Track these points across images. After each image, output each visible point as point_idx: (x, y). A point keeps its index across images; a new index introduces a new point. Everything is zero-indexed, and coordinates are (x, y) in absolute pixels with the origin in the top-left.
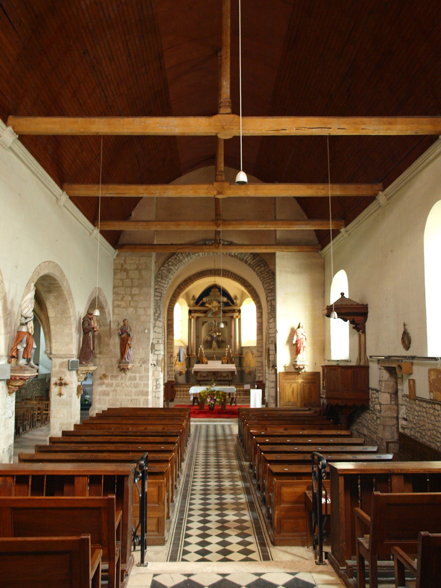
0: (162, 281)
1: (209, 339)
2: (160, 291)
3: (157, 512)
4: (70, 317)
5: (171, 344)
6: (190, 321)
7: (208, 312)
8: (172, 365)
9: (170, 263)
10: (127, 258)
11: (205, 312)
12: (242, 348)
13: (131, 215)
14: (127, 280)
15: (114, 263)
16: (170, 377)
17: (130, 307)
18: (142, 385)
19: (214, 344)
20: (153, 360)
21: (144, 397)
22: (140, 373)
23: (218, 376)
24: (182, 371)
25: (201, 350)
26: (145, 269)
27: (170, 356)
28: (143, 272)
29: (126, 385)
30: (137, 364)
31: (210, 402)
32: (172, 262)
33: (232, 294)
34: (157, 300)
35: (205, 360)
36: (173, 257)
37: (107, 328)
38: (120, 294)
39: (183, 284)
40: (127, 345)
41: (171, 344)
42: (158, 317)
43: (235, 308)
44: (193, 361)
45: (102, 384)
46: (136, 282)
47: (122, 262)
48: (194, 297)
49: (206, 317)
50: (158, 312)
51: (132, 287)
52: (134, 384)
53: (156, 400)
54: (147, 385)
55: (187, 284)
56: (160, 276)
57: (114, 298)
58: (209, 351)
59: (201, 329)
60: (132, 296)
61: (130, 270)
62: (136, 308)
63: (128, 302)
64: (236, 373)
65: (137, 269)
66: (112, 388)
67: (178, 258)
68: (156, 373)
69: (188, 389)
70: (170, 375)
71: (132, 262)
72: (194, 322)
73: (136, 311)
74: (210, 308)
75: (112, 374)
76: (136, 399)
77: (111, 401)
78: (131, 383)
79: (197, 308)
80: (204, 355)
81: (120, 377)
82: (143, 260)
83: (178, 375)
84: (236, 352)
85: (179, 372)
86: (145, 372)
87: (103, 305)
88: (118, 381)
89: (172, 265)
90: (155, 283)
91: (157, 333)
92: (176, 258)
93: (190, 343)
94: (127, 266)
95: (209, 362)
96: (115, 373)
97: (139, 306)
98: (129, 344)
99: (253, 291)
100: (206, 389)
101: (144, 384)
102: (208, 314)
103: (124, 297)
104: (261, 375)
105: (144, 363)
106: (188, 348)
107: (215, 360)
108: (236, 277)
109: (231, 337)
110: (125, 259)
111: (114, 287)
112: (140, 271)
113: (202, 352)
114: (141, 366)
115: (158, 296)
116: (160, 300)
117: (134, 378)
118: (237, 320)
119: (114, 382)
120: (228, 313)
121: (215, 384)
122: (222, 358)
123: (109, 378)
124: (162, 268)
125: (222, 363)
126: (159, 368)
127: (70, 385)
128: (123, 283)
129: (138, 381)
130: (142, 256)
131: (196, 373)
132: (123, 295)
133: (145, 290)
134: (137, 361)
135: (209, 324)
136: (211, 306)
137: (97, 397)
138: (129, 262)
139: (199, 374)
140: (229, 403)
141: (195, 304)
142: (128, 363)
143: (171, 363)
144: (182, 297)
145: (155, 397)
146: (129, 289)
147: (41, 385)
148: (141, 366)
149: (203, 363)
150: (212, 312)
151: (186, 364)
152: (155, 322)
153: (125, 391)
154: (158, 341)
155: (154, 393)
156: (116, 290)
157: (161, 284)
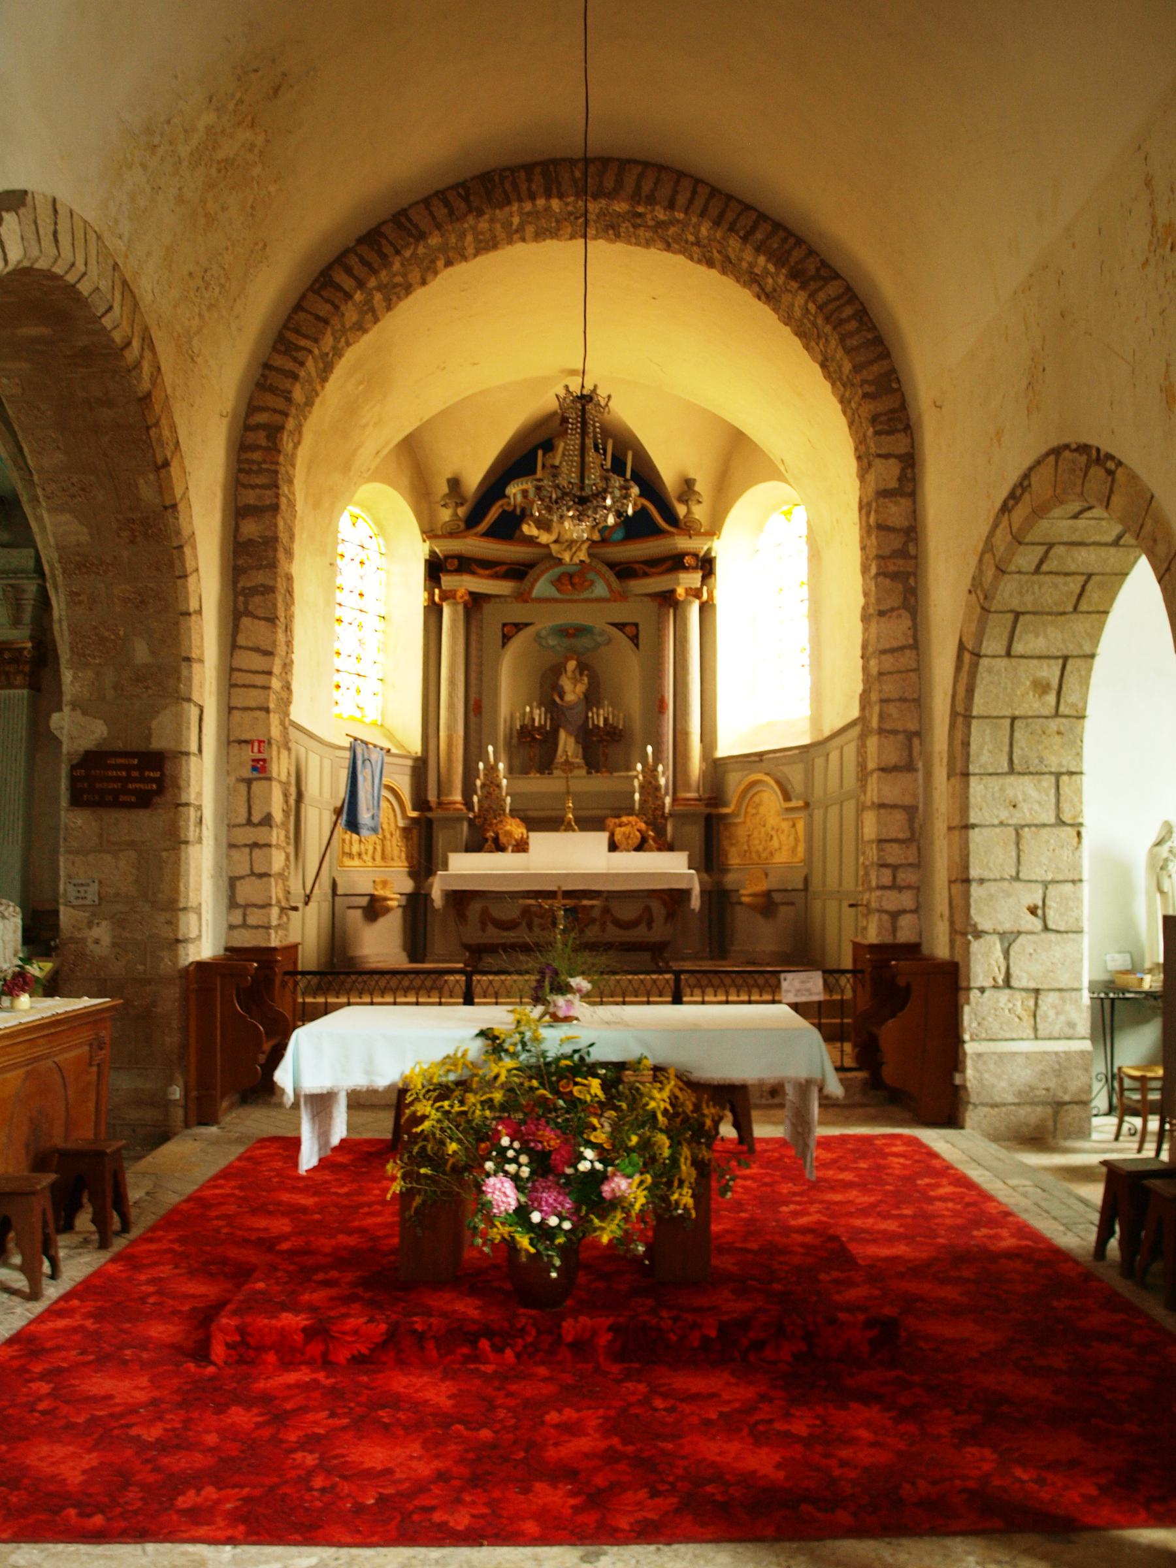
1: (539, 716)
5: (259, 680)
6: (433, 619)
7: (532, 574)
8: (259, 835)
11: (518, 572)
12: (717, 768)
16: (244, 925)
19: (567, 744)
24: (380, 892)
25: (492, 769)
27: (247, 773)
31: (522, 1212)
33: (668, 475)
35: (516, 829)
39: (353, 260)
41: (259, 680)
43: (683, 543)
44: (441, 838)
48: (455, 484)
49: (522, 597)
55: (386, 262)
58: (536, 784)
64: (695, 903)
72: (454, 621)
74: (547, 546)
79: (473, 545)
80: (508, 799)
84: (687, 787)
85: (364, 901)
93: (432, 746)
95: (537, 840)
99: (848, 311)
100: (475, 1048)
102: (536, 580)
104: (906, 900)
106: (420, 769)
107: (569, 828)
108: (730, 216)
109: (661, 706)
113: (499, 786)
118: (694, 612)
120: (646, 575)
121: (580, 982)
122: (611, 822)
125: (613, 847)
131: (459, 899)
135: (538, 637)
136: (553, 537)
139: (475, 907)
141: (462, 526)
143: (256, 818)
149: (499, 848)
150: (558, 570)
151: (409, 858)
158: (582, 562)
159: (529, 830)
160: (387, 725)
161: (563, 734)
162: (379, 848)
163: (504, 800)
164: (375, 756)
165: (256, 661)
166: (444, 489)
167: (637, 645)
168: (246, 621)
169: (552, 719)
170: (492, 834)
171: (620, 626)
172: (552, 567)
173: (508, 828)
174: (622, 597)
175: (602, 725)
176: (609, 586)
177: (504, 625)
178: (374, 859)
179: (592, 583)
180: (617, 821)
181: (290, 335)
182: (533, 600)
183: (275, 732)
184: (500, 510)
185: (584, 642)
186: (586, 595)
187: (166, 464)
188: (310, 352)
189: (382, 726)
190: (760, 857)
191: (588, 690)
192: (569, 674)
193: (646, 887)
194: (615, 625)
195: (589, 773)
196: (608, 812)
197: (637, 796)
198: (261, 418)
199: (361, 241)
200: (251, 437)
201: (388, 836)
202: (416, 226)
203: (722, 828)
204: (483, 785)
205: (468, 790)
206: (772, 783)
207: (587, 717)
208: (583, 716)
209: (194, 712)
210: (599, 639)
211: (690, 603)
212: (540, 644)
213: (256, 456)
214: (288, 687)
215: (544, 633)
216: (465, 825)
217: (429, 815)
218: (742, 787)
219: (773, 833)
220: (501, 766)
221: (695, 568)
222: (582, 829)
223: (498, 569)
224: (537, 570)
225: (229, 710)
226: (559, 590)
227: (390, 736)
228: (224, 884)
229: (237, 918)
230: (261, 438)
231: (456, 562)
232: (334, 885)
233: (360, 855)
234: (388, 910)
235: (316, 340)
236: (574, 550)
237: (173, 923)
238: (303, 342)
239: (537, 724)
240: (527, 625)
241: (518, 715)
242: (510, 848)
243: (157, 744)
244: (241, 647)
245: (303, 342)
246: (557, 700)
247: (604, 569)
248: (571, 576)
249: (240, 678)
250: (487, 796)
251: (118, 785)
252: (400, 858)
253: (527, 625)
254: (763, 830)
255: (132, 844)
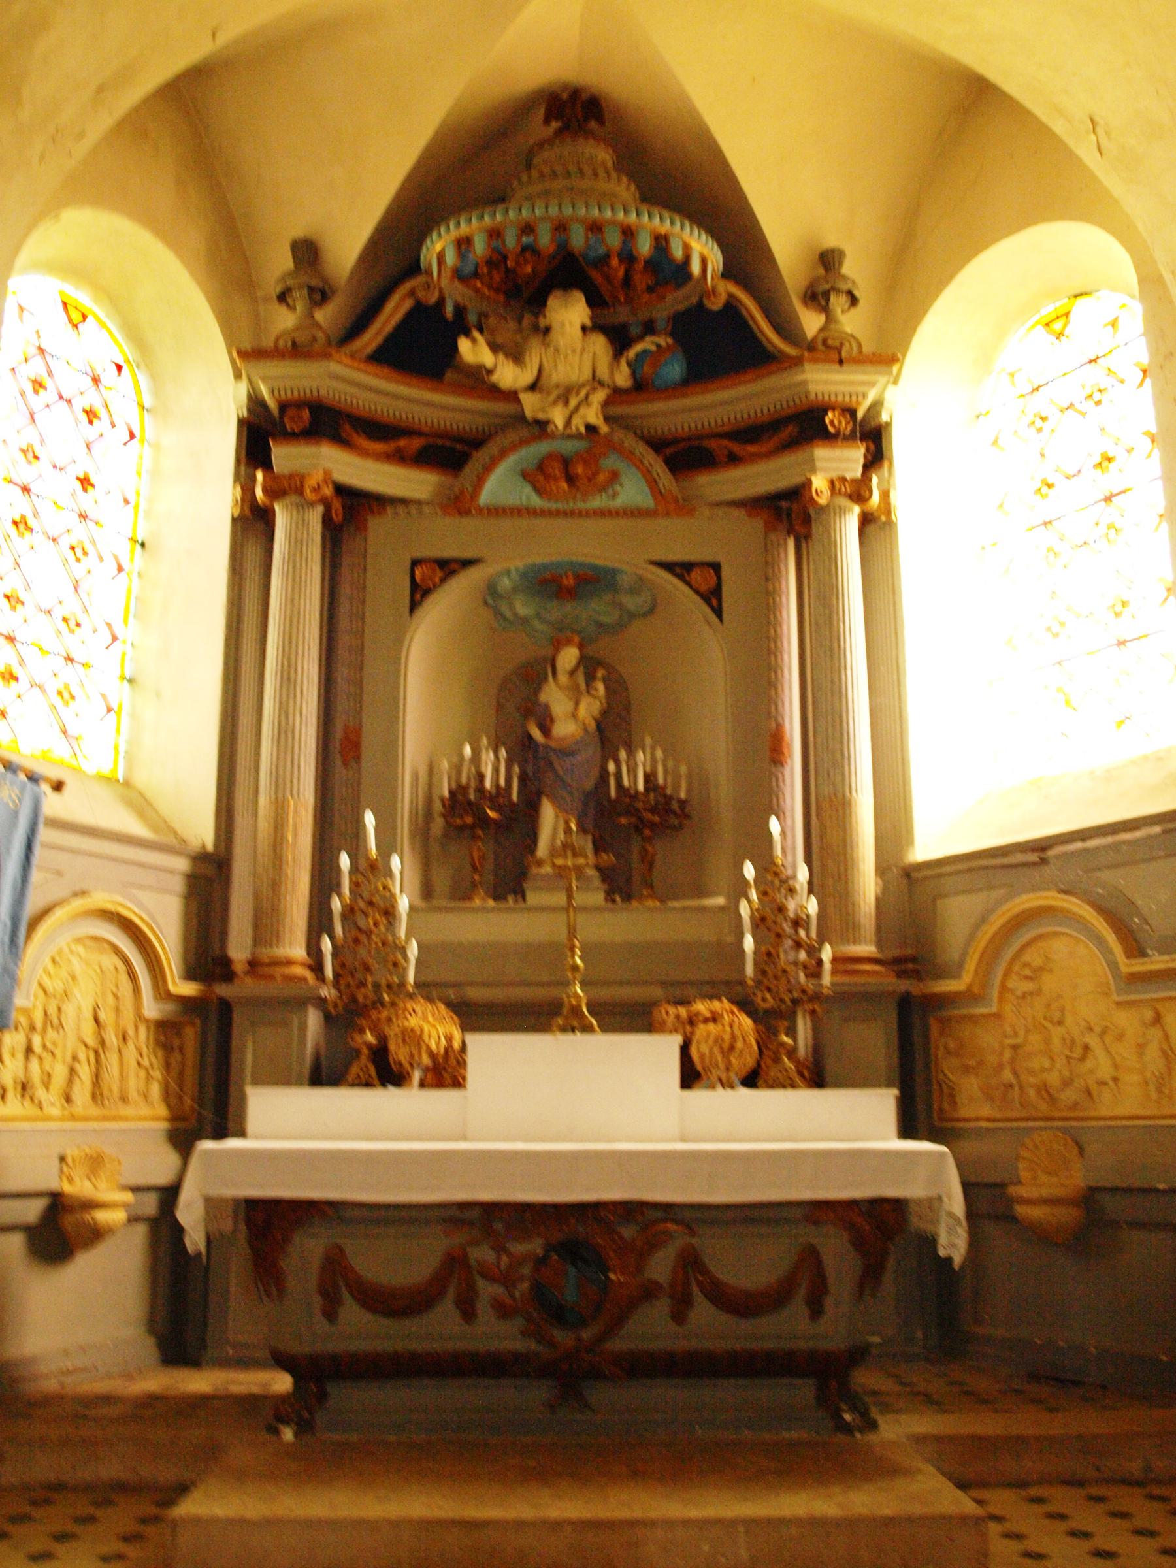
3: (923, 1362)
6: (253, 553)
7: (479, 458)
23: (650, 1292)
24: (78, 1187)
59: (399, 640)
72: (296, 543)
74: (512, 396)
80: (413, 950)
85: (32, 1211)
102: (488, 469)
107: (574, 1023)
113: (389, 913)
120: (734, 460)
125: (690, 1077)
135: (491, 589)
136: (528, 377)
140: (499, 1258)
158: (591, 429)
159: (466, 1027)
160: (141, 780)
161: (548, 814)
162: (85, 1072)
163: (403, 951)
166: (284, 261)
167: (718, 612)
169: (523, 779)
170: (369, 1037)
171: (680, 569)
172: (524, 442)
173: (413, 1022)
174: (682, 507)
175: (641, 786)
176: (653, 483)
177: (415, 563)
178: (68, 1099)
179: (614, 476)
180: (683, 1011)
182: (480, 510)
184: (408, 304)
185: (597, 609)
186: (598, 502)
189: (127, 784)
190: (1052, 1100)
191: (604, 713)
192: (563, 678)
193: (807, 1195)
194: (669, 567)
195: (609, 896)
196: (658, 992)
197: (749, 943)
201: (112, 1038)
203: (935, 1030)
204: (349, 913)
205: (319, 922)
206: (1087, 912)
207: (604, 776)
208: (595, 773)
210: (630, 602)
211: (842, 511)
212: (498, 613)
215: (506, 583)
216: (313, 1019)
217: (223, 990)
218: (989, 931)
219: (1093, 1041)
220: (396, 862)
221: (851, 438)
222: (606, 1028)
223: (402, 443)
224: (492, 449)
226: (539, 491)
231: (306, 414)
233: (24, 1087)
234: (96, 1234)
236: (573, 402)
239: (488, 784)
240: (467, 563)
241: (445, 765)
242: (417, 1076)
246: (536, 733)
247: (641, 449)
248: (566, 463)
250: (357, 936)
252: (146, 1096)
253: (467, 563)
254: (1057, 1033)
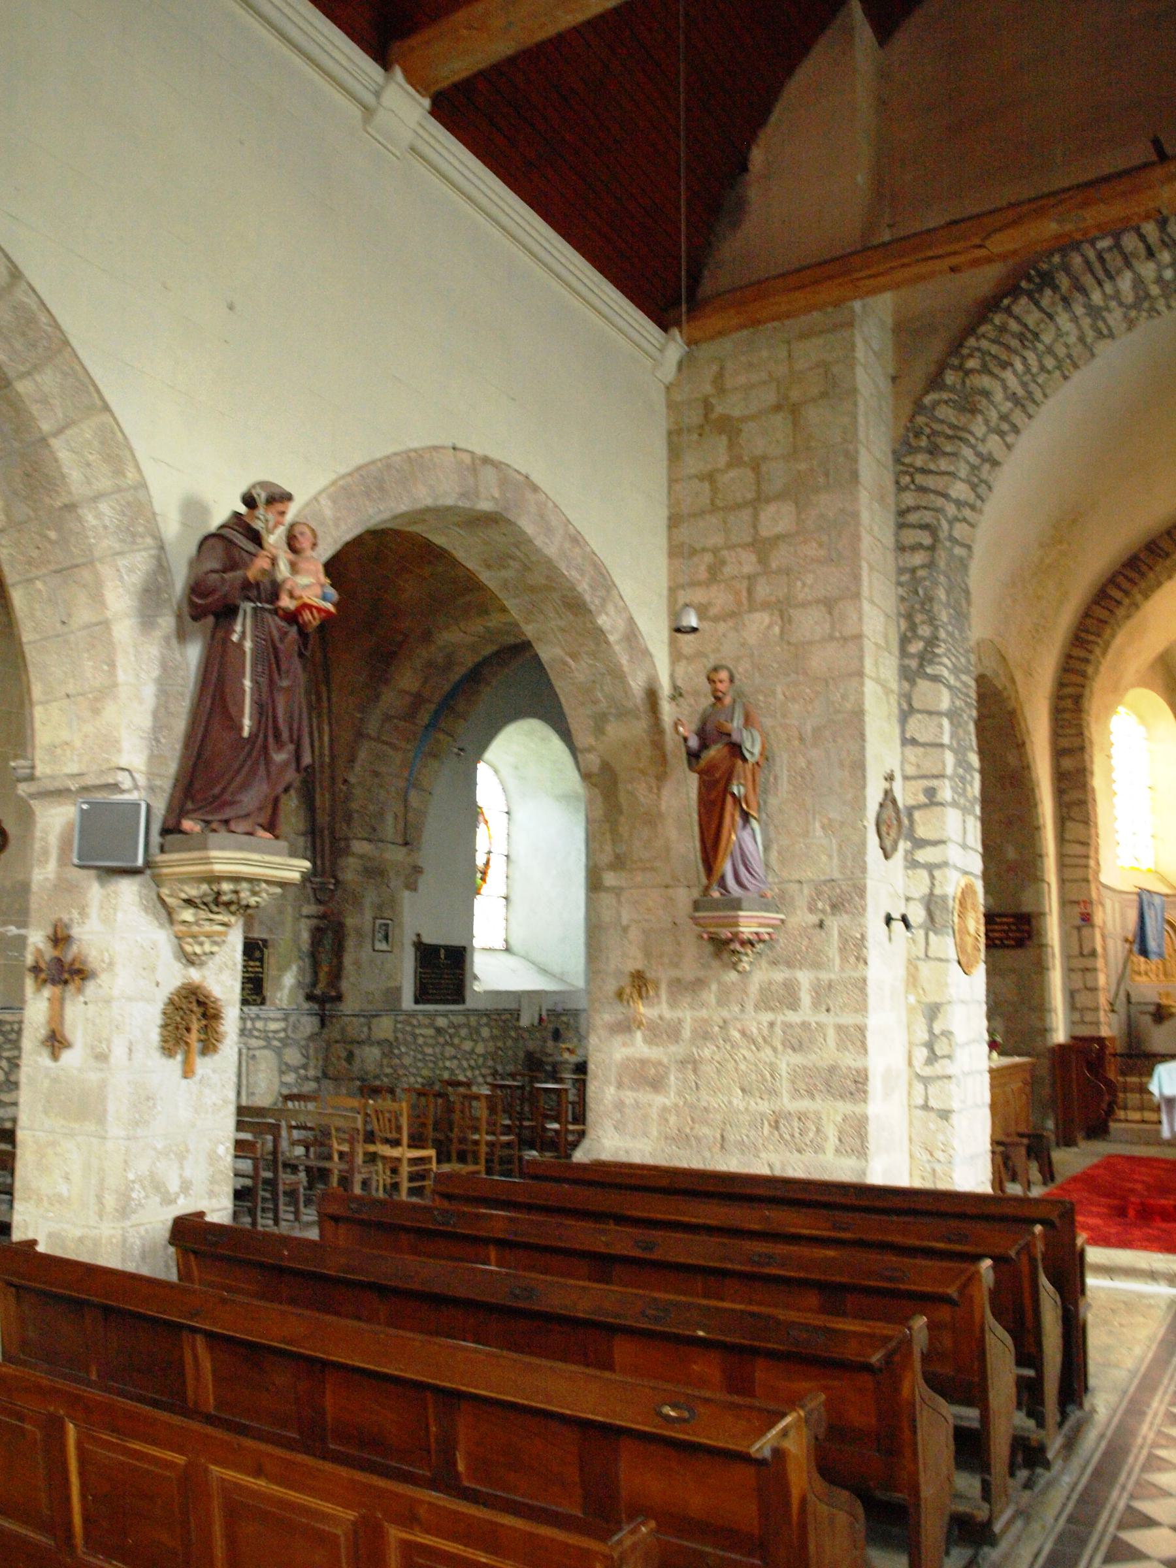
0: (932, 467)
2: (927, 517)
4: (71, 507)
5: (1082, 861)
8: (1088, 963)
9: (971, 364)
10: (729, 365)
13: (745, 169)
14: (732, 474)
15: (671, 405)
16: (1083, 1022)
17: (752, 609)
18: (831, 1033)
20: (908, 899)
21: (846, 1107)
22: (817, 965)
24: (1164, 1002)
26: (824, 395)
27: (1078, 922)
28: (813, 415)
29: (743, 1033)
30: (802, 918)
32: (985, 353)
34: (913, 571)
36: (983, 329)
37: (640, 727)
38: (704, 550)
39: (1120, 579)
40: (729, 799)
41: (1082, 861)
42: (927, 657)
45: (625, 1027)
46: (778, 474)
47: (708, 389)
50: (925, 631)
51: (759, 501)
52: (788, 1026)
53: (932, 1126)
54: (856, 1038)
55: (1143, 575)
56: (924, 443)
57: (673, 574)
60: (762, 547)
61: (744, 419)
62: (782, 609)
63: (745, 583)
65: (778, 408)
66: (678, 1050)
67: (1014, 326)
68: (926, 970)
69: (1144, 1080)
70: (1082, 1010)
71: (755, 378)
73: (786, 620)
75: (675, 973)
76: (802, 1117)
77: (672, 1119)
78: (772, 1024)
81: (714, 987)
82: (810, 352)
83: (1147, 1020)
85: (1152, 1009)
86: (844, 959)
87: (573, 589)
88: (704, 1013)
89: (985, 370)
90: (897, 482)
91: (924, 745)
92: (1003, 329)
94: (732, 406)
96: (689, 971)
97: (801, 596)
98: (737, 800)
101: (840, 1028)
103: (723, 563)
105: (835, 907)
110: (720, 375)
111: (674, 521)
112: (795, 411)
114: (821, 925)
115: (914, 548)
116: (931, 565)
117: (789, 997)
119: (687, 1016)
123: (664, 996)
124: (927, 400)
126: (945, 945)
127: (104, 978)
128: (714, 490)
129: (805, 1013)
130: (804, 336)
132: (715, 551)
133: (827, 503)
134: (801, 902)
137: (610, 1092)
138: (742, 380)
142: (736, 905)
144: (1143, 683)
145: (926, 1107)
146: (746, 515)
147: (493, 1038)
148: (821, 925)
152: (906, 685)
153: (743, 1067)
154: (931, 792)
155: (919, 1087)
156: (684, 533)
157: (929, 481)
164: (1157, 900)
165: (1077, 849)
168: (1069, 824)
181: (1083, 635)
183: (1094, 895)
187: (1024, 744)
188: (1096, 643)
198: (1069, 690)
199: (1124, 565)
200: (1063, 704)
202: (1162, 550)
209: (1046, 886)
213: (1067, 716)
214: (1098, 864)
225: (1062, 881)
227: (1163, 879)
228: (1068, 994)
229: (1077, 1017)
230: (1069, 704)
232: (1128, 996)
235: (1099, 635)
237: (1042, 1019)
238: (1092, 638)
243: (1027, 908)
244: (1069, 841)
245: (1092, 638)
249: (1068, 861)
251: (1003, 935)
255: (1013, 971)
